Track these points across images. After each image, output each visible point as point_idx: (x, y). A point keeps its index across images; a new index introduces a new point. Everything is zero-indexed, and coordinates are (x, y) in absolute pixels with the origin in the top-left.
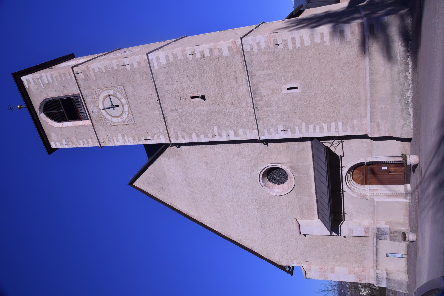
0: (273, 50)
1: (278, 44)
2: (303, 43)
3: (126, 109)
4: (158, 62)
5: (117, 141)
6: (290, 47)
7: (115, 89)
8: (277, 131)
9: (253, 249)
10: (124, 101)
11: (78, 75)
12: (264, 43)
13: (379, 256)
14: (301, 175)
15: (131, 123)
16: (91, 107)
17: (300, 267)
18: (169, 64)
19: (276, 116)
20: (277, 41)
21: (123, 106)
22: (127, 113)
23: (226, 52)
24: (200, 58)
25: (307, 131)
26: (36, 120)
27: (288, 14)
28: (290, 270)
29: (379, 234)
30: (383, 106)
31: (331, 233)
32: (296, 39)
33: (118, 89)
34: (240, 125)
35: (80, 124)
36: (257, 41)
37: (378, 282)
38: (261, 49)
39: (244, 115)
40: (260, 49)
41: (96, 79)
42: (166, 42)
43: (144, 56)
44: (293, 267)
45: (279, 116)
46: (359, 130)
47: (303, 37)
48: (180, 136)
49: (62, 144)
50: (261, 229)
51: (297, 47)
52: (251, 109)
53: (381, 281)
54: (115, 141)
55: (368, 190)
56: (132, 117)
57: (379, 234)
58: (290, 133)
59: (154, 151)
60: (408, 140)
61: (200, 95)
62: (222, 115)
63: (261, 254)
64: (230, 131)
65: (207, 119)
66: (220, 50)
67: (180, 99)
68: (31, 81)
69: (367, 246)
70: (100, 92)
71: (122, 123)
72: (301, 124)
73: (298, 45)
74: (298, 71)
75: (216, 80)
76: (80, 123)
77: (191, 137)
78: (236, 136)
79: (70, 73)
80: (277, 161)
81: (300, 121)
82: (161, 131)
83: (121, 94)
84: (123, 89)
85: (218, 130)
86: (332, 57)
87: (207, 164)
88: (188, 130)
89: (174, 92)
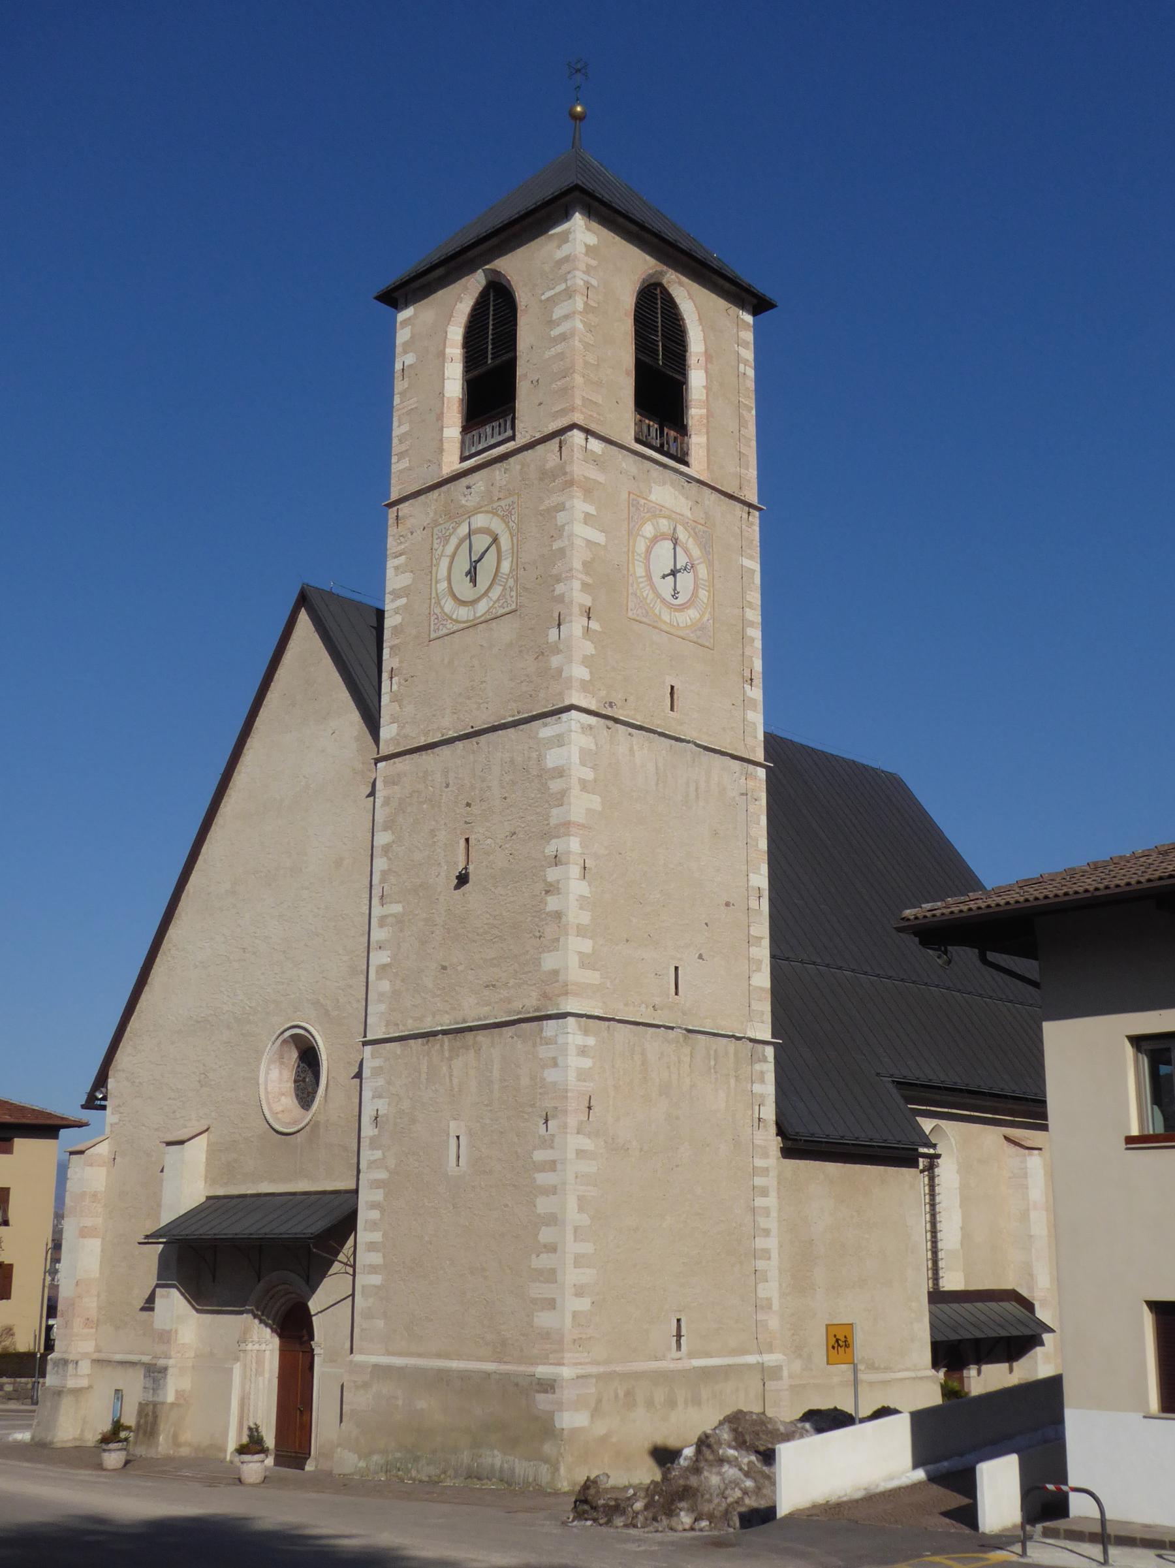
1: (546, 1122)
3: (463, 613)
6: (539, 1156)
7: (511, 582)
8: (378, 1096)
9: (147, 988)
18: (544, 775)
20: (554, 1117)
23: (549, 962)
29: (155, 1373)
33: (511, 590)
37: (57, 1363)
46: (362, 1330)
55: (263, 1347)
56: (445, 631)
67: (468, 805)
68: (565, 250)
72: (386, 1168)
73: (543, 1178)
76: (453, 430)
77: (386, 828)
79: (563, 412)
80: (331, 1083)
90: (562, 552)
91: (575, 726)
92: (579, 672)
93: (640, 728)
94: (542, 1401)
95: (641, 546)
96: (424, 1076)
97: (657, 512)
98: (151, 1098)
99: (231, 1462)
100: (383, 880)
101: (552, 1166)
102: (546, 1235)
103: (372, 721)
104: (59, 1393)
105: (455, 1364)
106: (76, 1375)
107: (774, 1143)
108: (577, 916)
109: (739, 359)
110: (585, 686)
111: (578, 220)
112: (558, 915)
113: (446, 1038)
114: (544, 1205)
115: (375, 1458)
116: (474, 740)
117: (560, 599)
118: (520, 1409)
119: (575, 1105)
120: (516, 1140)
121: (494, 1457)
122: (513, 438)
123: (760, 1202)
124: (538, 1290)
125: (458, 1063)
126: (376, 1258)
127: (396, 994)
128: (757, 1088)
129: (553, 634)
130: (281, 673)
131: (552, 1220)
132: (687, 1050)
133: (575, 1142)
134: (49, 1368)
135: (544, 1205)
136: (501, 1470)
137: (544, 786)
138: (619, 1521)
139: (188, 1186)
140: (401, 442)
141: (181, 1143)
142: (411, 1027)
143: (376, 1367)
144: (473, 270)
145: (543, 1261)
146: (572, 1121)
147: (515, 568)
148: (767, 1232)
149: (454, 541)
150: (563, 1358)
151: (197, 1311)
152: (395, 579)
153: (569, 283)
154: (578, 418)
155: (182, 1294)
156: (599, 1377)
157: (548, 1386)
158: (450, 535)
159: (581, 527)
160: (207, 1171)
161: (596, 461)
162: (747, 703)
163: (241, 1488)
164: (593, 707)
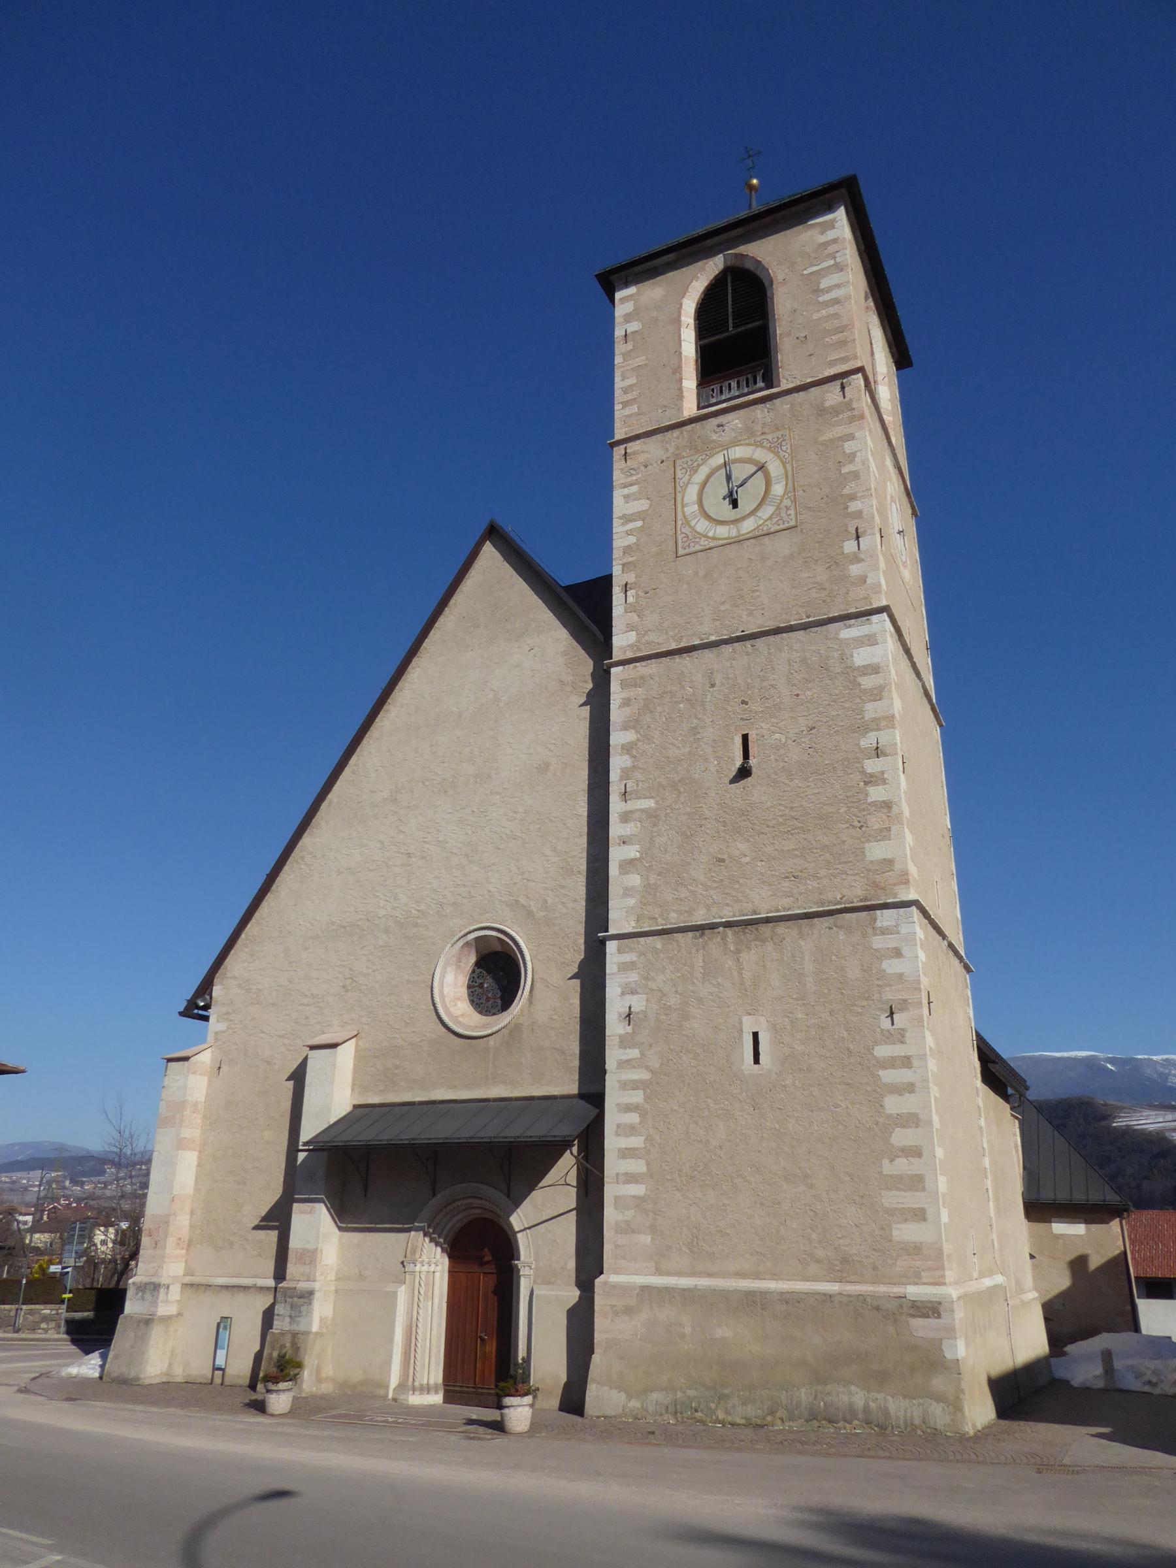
0: (876, 996)
1: (892, 1014)
2: (893, 1092)
3: (722, 531)
4: (861, 642)
5: (627, 498)
6: (883, 1051)
7: (787, 502)
10: (748, 526)
11: (838, 388)
12: (899, 971)
13: (224, 1292)
14: (491, 1056)
15: (680, 545)
16: (735, 421)
17: (205, 1042)
18: (852, 674)
19: (676, 992)
20: (901, 1010)
21: (735, 522)
22: (711, 534)
23: (876, 851)
24: (863, 772)
25: (625, 1086)
26: (709, 242)
27: (1005, 1049)
28: (197, 1008)
30: (688, 1330)
31: (305, 1144)
32: (904, 1071)
33: (788, 508)
34: (653, 878)
35: (685, 383)
36: (906, 951)
38: (880, 959)
39: (684, 893)
40: (880, 955)
41: (822, 445)
42: (925, 662)
43: (883, 596)
44: (206, 1019)
45: (673, 1001)
46: (617, 1246)
47: (912, 1091)
48: (631, 693)
49: (628, 318)
50: (333, 923)
51: (881, 1073)
52: (699, 918)
53: (143, 1299)
54: (626, 491)
55: (432, 1268)
56: (698, 547)
57: (291, 1297)
58: (622, 1032)
59: (586, 608)
61: (752, 762)
62: (689, 827)
63: (253, 920)
64: (637, 847)
65: (677, 777)
66: (884, 834)
67: (743, 702)
68: (830, 235)
69: (259, 1255)
70: (782, 454)
71: (680, 516)
72: (647, 1068)
73: (888, 1076)
74: (809, 1070)
75: (793, 814)
76: (690, 383)
77: (625, 728)
78: (620, 866)
79: (844, 360)
80: (538, 984)
81: (657, 1066)
82: (651, 637)
83: (770, 518)
84: (786, 525)
85: (642, 811)
86: (847, 1178)
87: (543, 768)
88: (647, 719)
89: (766, 683)
94: (921, 1327)
98: (273, 1005)
99: (395, 1400)
102: (901, 1137)
105: (772, 1285)
106: (167, 1302)
113: (729, 932)
114: (893, 1105)
115: (655, 1396)
116: (748, 644)
120: (845, 1034)
121: (850, 1393)
124: (891, 1199)
130: (458, 599)
131: (911, 1120)
136: (866, 1410)
139: (333, 1097)
141: (334, 1046)
143: (644, 1288)
144: (715, 255)
147: (792, 489)
150: (943, 1276)
151: (340, 1229)
153: (838, 260)
155: (328, 1210)
158: (699, 466)
160: (354, 1079)
163: (500, 1441)
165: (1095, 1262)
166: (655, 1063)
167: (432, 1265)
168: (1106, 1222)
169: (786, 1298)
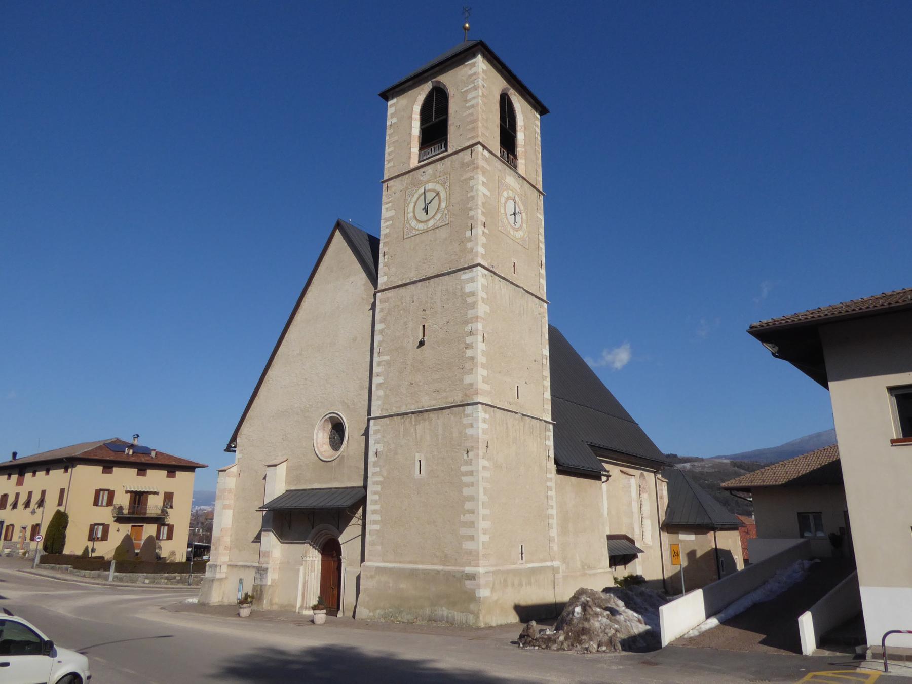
3: (421, 226)
6: (464, 469)
7: (446, 212)
8: (377, 442)
10: (431, 223)
18: (464, 296)
23: (468, 379)
28: (230, 448)
29: (261, 571)
35: (412, 150)
37: (211, 567)
49: (393, 116)
60: (354, 616)
61: (426, 338)
68: (474, 70)
73: (466, 479)
76: (415, 149)
77: (381, 322)
79: (473, 138)
82: (392, 278)
87: (355, 340)
90: (473, 198)
91: (480, 274)
92: (481, 250)
93: (504, 278)
94: (469, 584)
95: (503, 200)
96: (402, 433)
97: (508, 188)
100: (380, 345)
101: (471, 473)
102: (468, 505)
103: (373, 277)
104: (212, 580)
105: (420, 567)
107: (553, 467)
108: (481, 359)
109: (535, 132)
110: (483, 256)
111: (479, 58)
112: (472, 358)
113: (413, 416)
114: (466, 492)
115: (378, 611)
117: (472, 218)
118: (458, 589)
119: (482, 446)
122: (446, 151)
123: (550, 493)
124: (464, 531)
125: (419, 428)
126: (377, 517)
127: (386, 396)
128: (547, 443)
129: (468, 234)
131: (472, 498)
132: (522, 424)
133: (483, 462)
134: (207, 569)
135: (466, 492)
136: (447, 617)
137: (466, 301)
138: (554, 647)
139: (278, 486)
140: (389, 155)
141: (275, 465)
142: (394, 411)
143: (377, 568)
145: (468, 517)
146: (481, 453)
147: (448, 206)
148: (552, 507)
149: (416, 196)
152: (386, 213)
154: (480, 140)
156: (493, 572)
157: (472, 577)
159: (481, 188)
161: (486, 160)
162: (540, 274)
163: (313, 626)
164: (486, 265)
165: (699, 554)
166: (385, 474)
167: (314, 558)
168: (705, 533)
169: (426, 573)
